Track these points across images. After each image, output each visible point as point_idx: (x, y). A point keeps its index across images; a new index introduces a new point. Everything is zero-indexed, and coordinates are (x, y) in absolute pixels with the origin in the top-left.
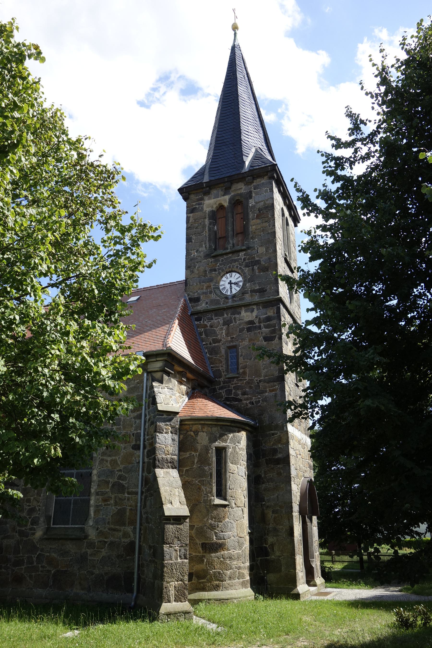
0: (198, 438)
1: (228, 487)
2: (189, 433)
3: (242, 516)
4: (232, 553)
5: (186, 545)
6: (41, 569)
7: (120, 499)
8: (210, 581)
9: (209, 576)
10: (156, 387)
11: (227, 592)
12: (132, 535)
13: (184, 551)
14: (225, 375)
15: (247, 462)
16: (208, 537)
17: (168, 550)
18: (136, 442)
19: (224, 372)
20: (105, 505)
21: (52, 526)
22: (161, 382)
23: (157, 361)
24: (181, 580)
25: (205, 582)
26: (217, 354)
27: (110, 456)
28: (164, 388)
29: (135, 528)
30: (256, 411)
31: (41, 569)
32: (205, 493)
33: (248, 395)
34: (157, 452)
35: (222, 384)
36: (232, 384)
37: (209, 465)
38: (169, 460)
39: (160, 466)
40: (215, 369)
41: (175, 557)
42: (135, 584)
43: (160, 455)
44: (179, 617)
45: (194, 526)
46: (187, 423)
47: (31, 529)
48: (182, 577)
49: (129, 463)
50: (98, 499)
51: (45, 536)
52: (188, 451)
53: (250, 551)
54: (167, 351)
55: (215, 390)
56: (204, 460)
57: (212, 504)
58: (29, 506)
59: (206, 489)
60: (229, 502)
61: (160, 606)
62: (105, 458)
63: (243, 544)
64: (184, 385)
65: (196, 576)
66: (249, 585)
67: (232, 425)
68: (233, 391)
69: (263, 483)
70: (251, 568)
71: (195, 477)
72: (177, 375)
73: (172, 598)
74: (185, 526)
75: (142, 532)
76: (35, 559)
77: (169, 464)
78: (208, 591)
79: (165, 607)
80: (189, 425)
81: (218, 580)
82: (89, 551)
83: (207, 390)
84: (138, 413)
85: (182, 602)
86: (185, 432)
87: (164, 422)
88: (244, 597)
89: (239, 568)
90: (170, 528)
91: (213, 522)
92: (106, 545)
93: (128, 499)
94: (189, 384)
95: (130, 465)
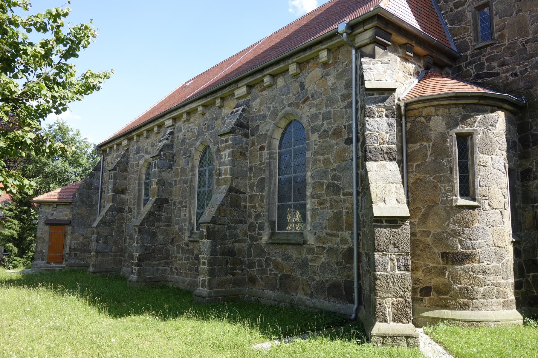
0: (432, 124)
1: (477, 183)
2: (418, 119)
3: (500, 220)
4: (487, 266)
5: (407, 253)
6: (269, 272)
7: (336, 201)
8: (454, 298)
9: (452, 292)
10: (365, 63)
11: (480, 312)
12: (350, 241)
13: (404, 261)
14: (474, 46)
15: (508, 151)
16: (450, 246)
17: (380, 259)
18: (349, 135)
19: (471, 42)
20: (321, 208)
21: (277, 231)
22: (373, 56)
23: (366, 30)
24: (401, 297)
25: (447, 299)
26: (460, 21)
27: (322, 155)
28: (377, 63)
29: (352, 233)
30: (521, 84)
31: (269, 272)
32: (443, 191)
33: (508, 65)
34: (368, 141)
35: (469, 59)
36: (484, 56)
37: (448, 156)
38: (385, 151)
39: (373, 158)
40: (458, 41)
41: (391, 267)
42: (356, 294)
43: (371, 145)
44: (399, 342)
45: (430, 232)
46: (414, 106)
47: (259, 234)
48: (402, 293)
49: (343, 161)
50: (314, 203)
51: (270, 241)
52: (418, 142)
53: (514, 264)
54: (375, 12)
55: (460, 68)
56: (441, 151)
57: (454, 204)
58: (255, 212)
59: (444, 187)
60: (479, 202)
61: (373, 325)
62: (318, 157)
63: (502, 255)
64: (412, 63)
65: (435, 291)
66: (514, 306)
67: (481, 102)
68: (486, 64)
69: (534, 179)
70: (518, 286)
71: (428, 173)
72: (400, 50)
73: (390, 317)
74: (405, 230)
75: (361, 237)
76: (264, 262)
77: (386, 156)
78: (452, 310)
79: (379, 328)
80: (418, 109)
81: (466, 298)
82: (309, 257)
83: (447, 69)
84: (349, 100)
85: (403, 323)
86: (413, 119)
87: (375, 103)
88: (505, 321)
89: (498, 285)
90: (383, 234)
91: (456, 228)
92: (325, 251)
93: (344, 201)
94: (420, 62)
95: (344, 163)
